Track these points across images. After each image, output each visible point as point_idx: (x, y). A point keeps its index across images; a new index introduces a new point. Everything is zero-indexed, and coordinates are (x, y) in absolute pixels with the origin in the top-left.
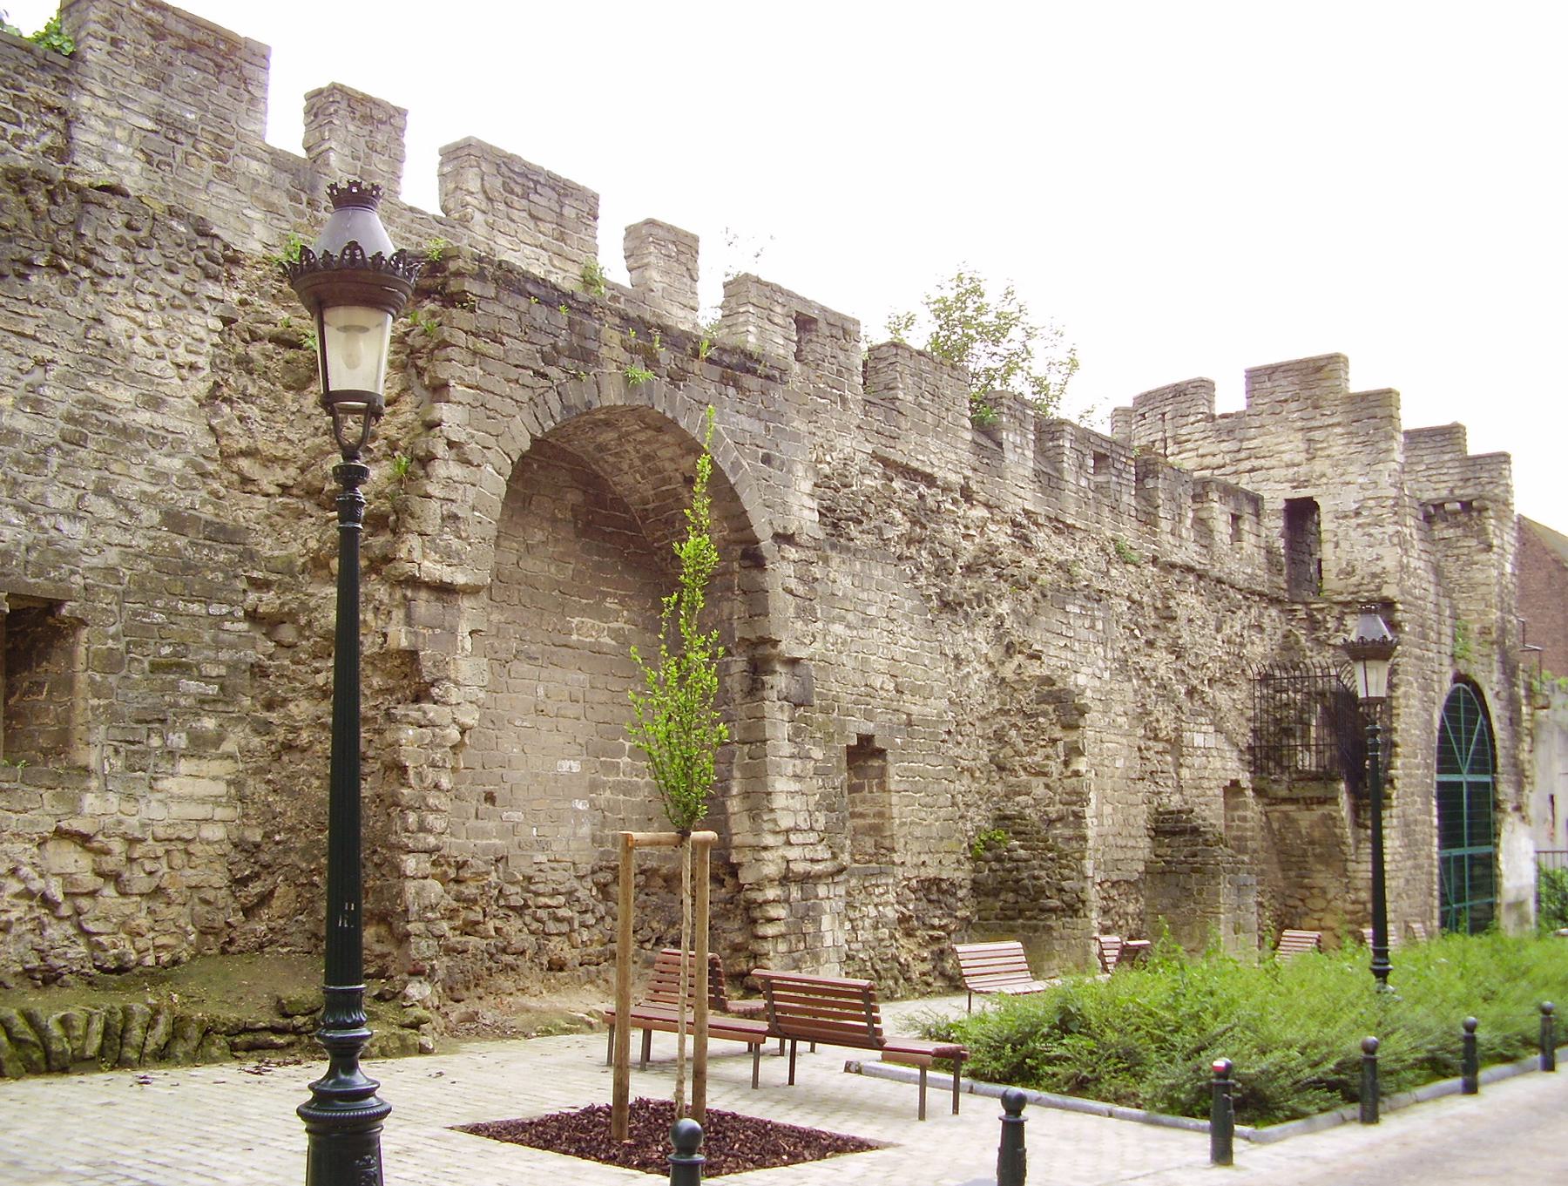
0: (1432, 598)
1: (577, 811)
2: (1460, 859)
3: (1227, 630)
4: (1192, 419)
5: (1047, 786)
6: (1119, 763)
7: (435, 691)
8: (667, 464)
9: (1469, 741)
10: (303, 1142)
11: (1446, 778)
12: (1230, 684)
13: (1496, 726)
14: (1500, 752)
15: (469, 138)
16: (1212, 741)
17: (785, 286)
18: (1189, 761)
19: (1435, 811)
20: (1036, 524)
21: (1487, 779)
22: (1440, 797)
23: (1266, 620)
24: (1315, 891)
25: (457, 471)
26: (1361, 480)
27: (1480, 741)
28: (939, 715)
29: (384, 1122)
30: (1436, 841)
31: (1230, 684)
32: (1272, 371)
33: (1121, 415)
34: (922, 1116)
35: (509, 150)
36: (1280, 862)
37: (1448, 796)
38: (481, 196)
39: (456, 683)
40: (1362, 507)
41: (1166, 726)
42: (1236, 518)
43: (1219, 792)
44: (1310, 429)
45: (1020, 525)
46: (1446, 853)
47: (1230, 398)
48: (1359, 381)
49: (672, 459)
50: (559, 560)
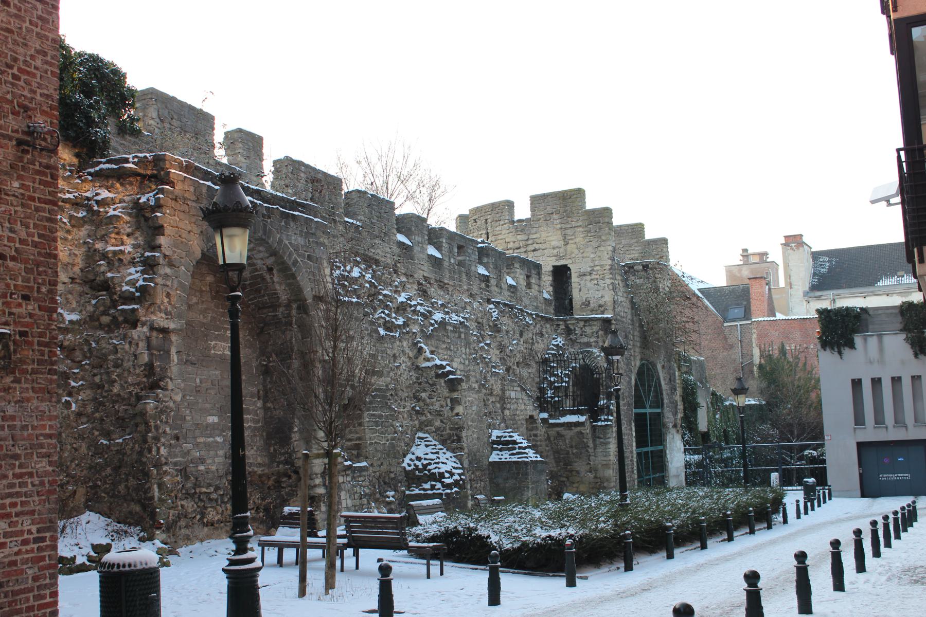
0: (629, 317)
1: (217, 442)
2: (647, 453)
3: (525, 336)
4: (502, 222)
5: (442, 421)
6: (474, 408)
7: (162, 383)
8: (259, 262)
9: (649, 391)
10: (225, 582)
11: (639, 411)
12: (527, 364)
13: (663, 383)
14: (665, 396)
15: (152, 89)
16: (519, 396)
17: (306, 162)
18: (508, 406)
19: (634, 429)
20: (430, 283)
21: (659, 410)
22: (636, 421)
23: (544, 330)
24: (574, 473)
25: (168, 270)
26: (592, 256)
27: (656, 391)
28: (387, 386)
29: (260, 573)
30: (634, 444)
31: (527, 364)
32: (544, 197)
33: (462, 219)
34: (428, 577)
35: (171, 94)
36: (555, 458)
37: (640, 420)
38: (158, 120)
39: (171, 379)
40: (593, 270)
41: (497, 389)
42: (528, 277)
43: (524, 422)
44: (566, 229)
45: (421, 284)
46: (640, 450)
47: (522, 211)
48: (591, 203)
49: (262, 259)
50: (204, 312)
